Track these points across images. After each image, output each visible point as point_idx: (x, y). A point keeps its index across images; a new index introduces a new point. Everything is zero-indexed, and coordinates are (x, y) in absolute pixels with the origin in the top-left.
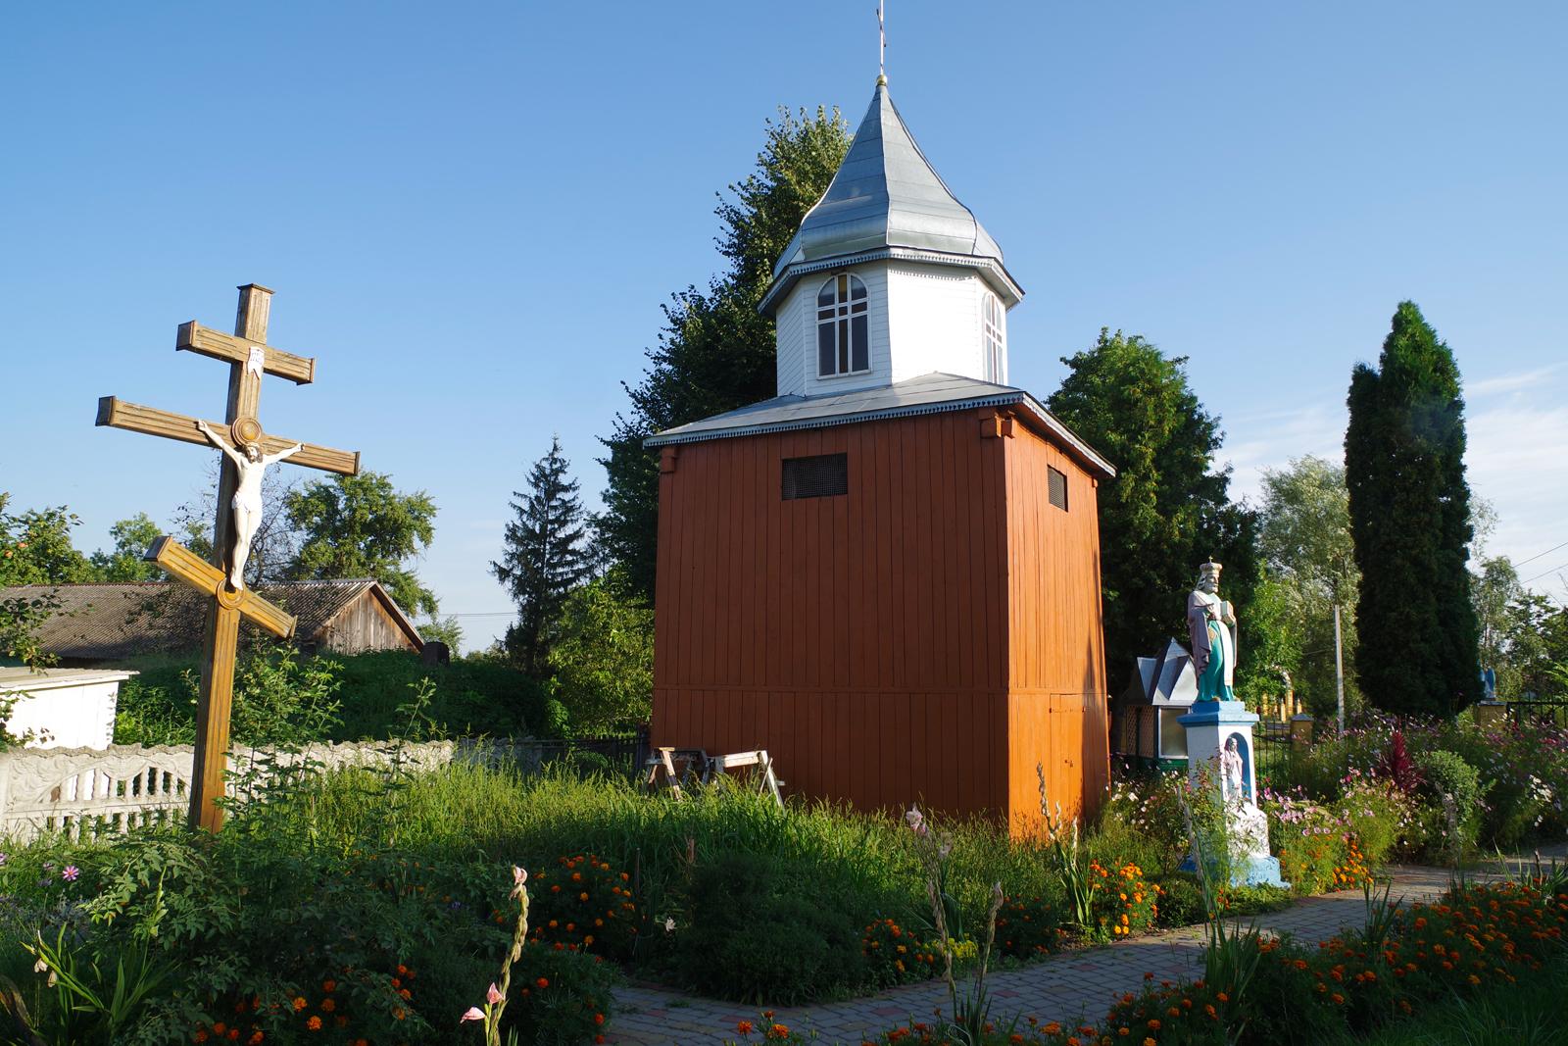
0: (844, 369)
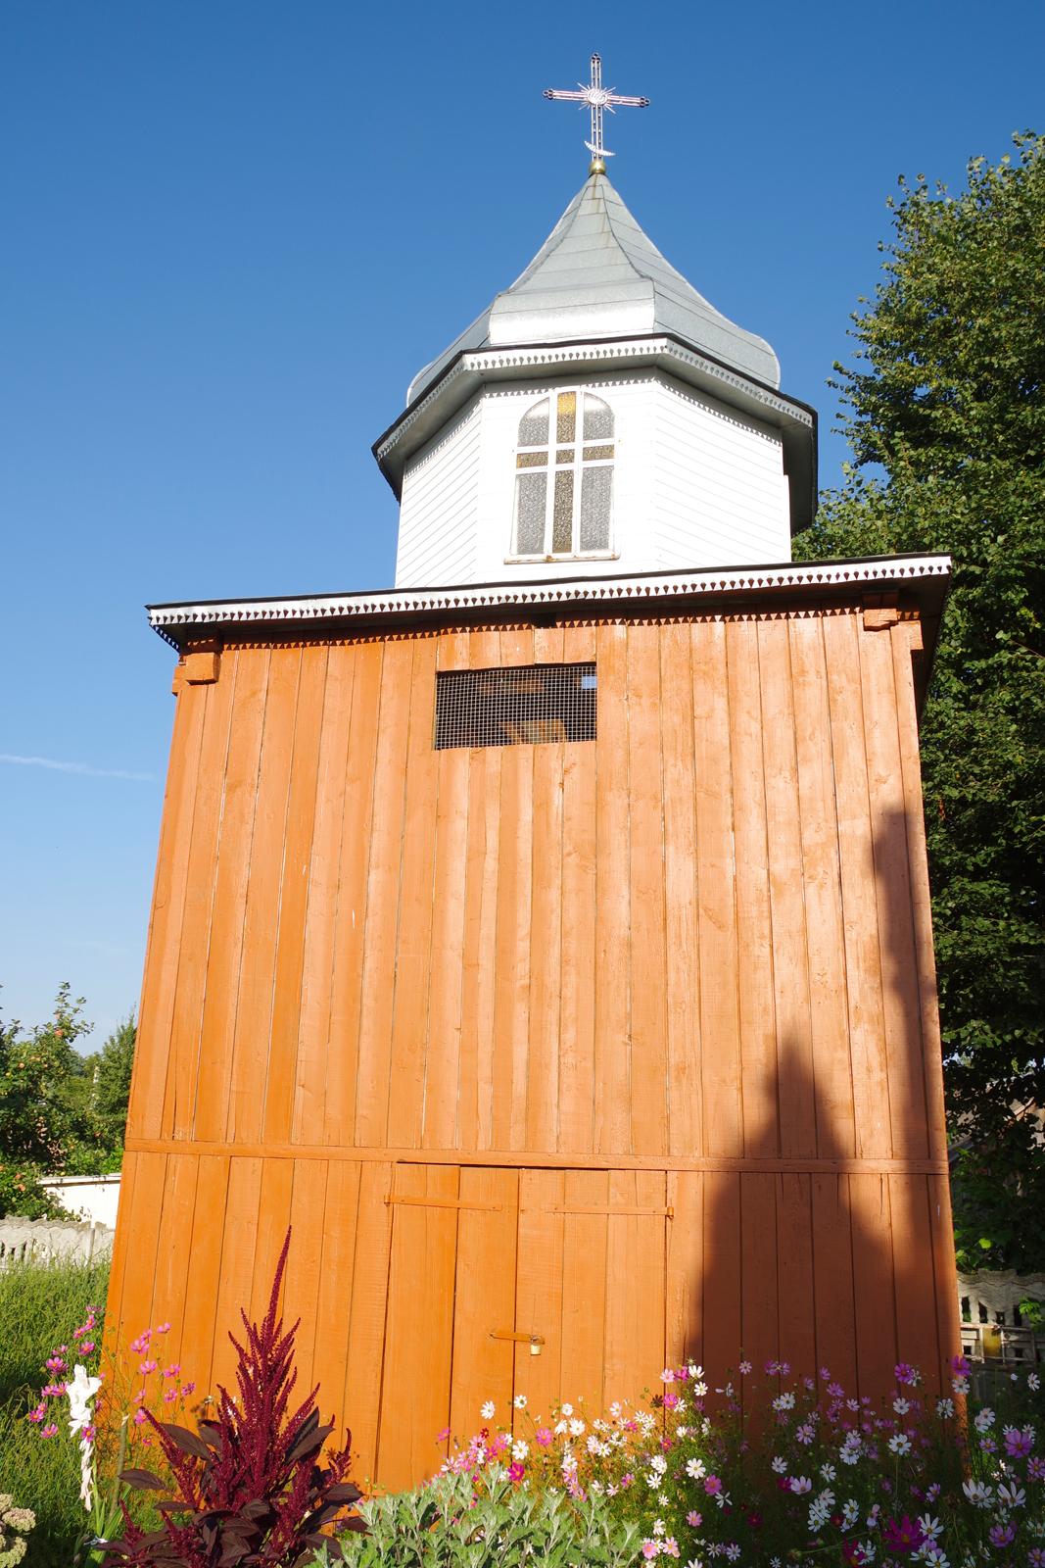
0: (562, 544)
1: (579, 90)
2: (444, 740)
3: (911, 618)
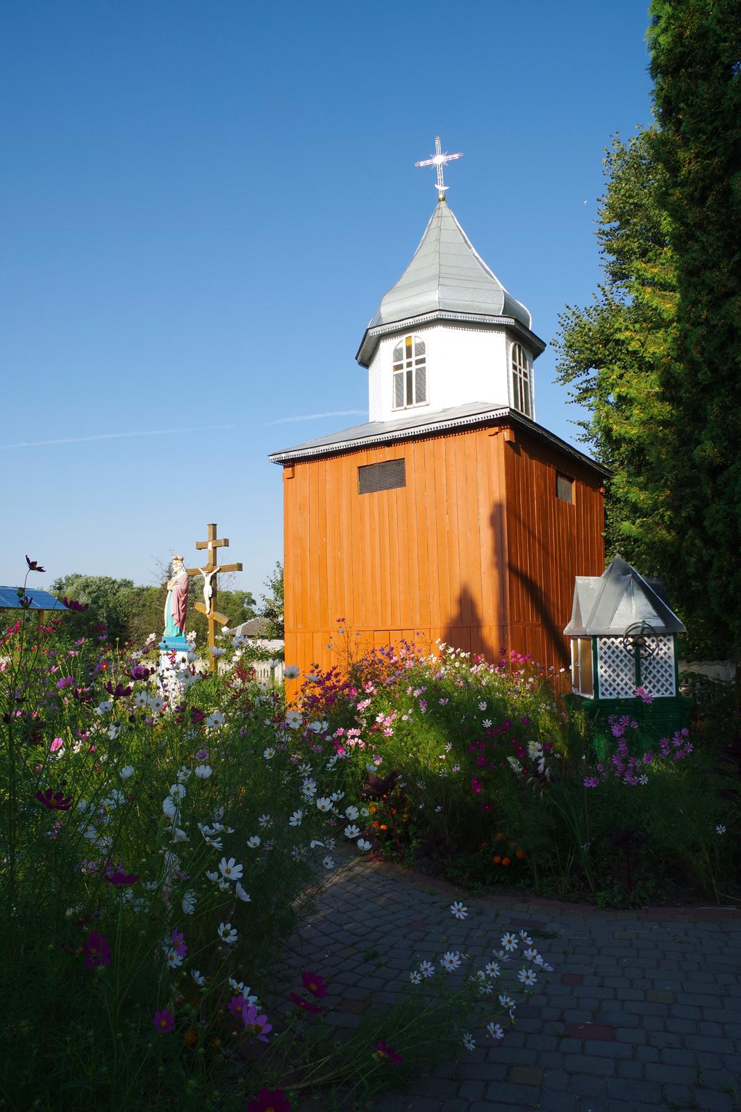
0: (410, 401)
1: (431, 158)
2: (361, 493)
3: (507, 428)
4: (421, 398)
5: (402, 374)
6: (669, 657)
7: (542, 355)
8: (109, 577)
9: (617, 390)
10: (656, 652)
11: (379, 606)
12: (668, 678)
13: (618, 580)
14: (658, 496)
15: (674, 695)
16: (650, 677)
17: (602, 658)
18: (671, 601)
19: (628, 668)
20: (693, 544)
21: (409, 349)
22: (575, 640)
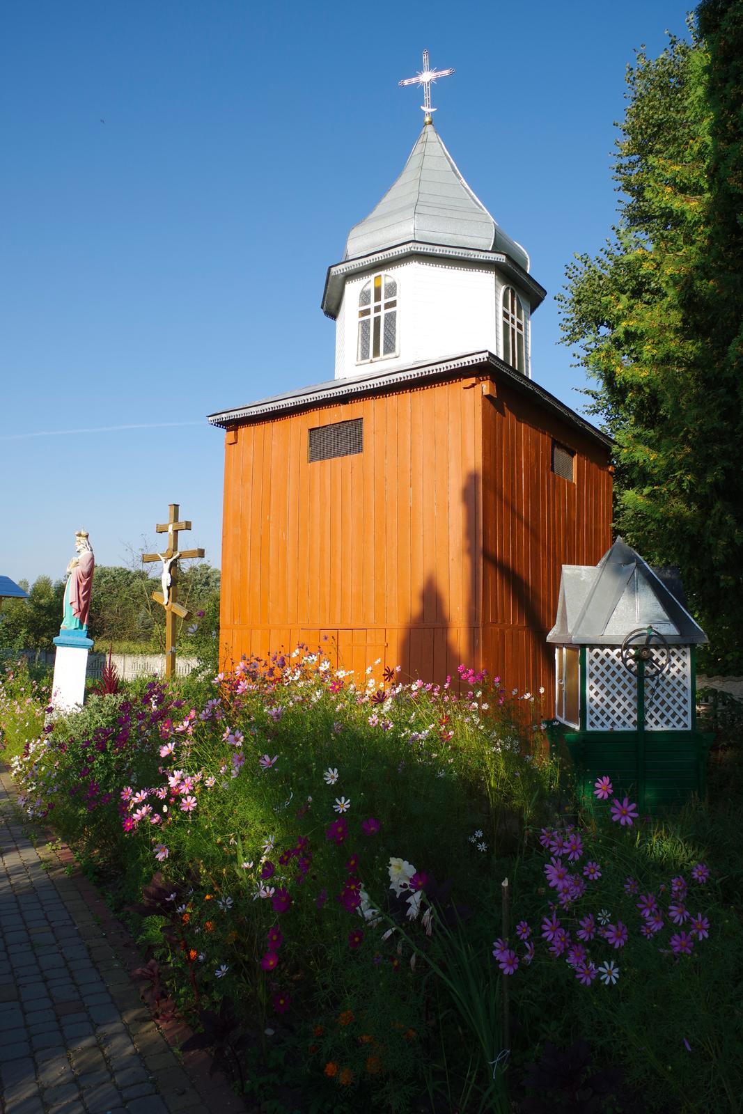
0: (376, 353)
1: (417, 75)
2: (311, 460)
3: (487, 379)
4: (390, 348)
5: (369, 320)
6: (684, 677)
7: (541, 305)
8: (123, 567)
9: (624, 324)
10: (666, 669)
11: (327, 598)
12: (682, 705)
13: (618, 571)
14: (674, 454)
15: (689, 728)
16: (657, 703)
17: (592, 675)
18: (690, 603)
19: (627, 690)
20: (721, 523)
21: (378, 291)
22: (561, 649)
